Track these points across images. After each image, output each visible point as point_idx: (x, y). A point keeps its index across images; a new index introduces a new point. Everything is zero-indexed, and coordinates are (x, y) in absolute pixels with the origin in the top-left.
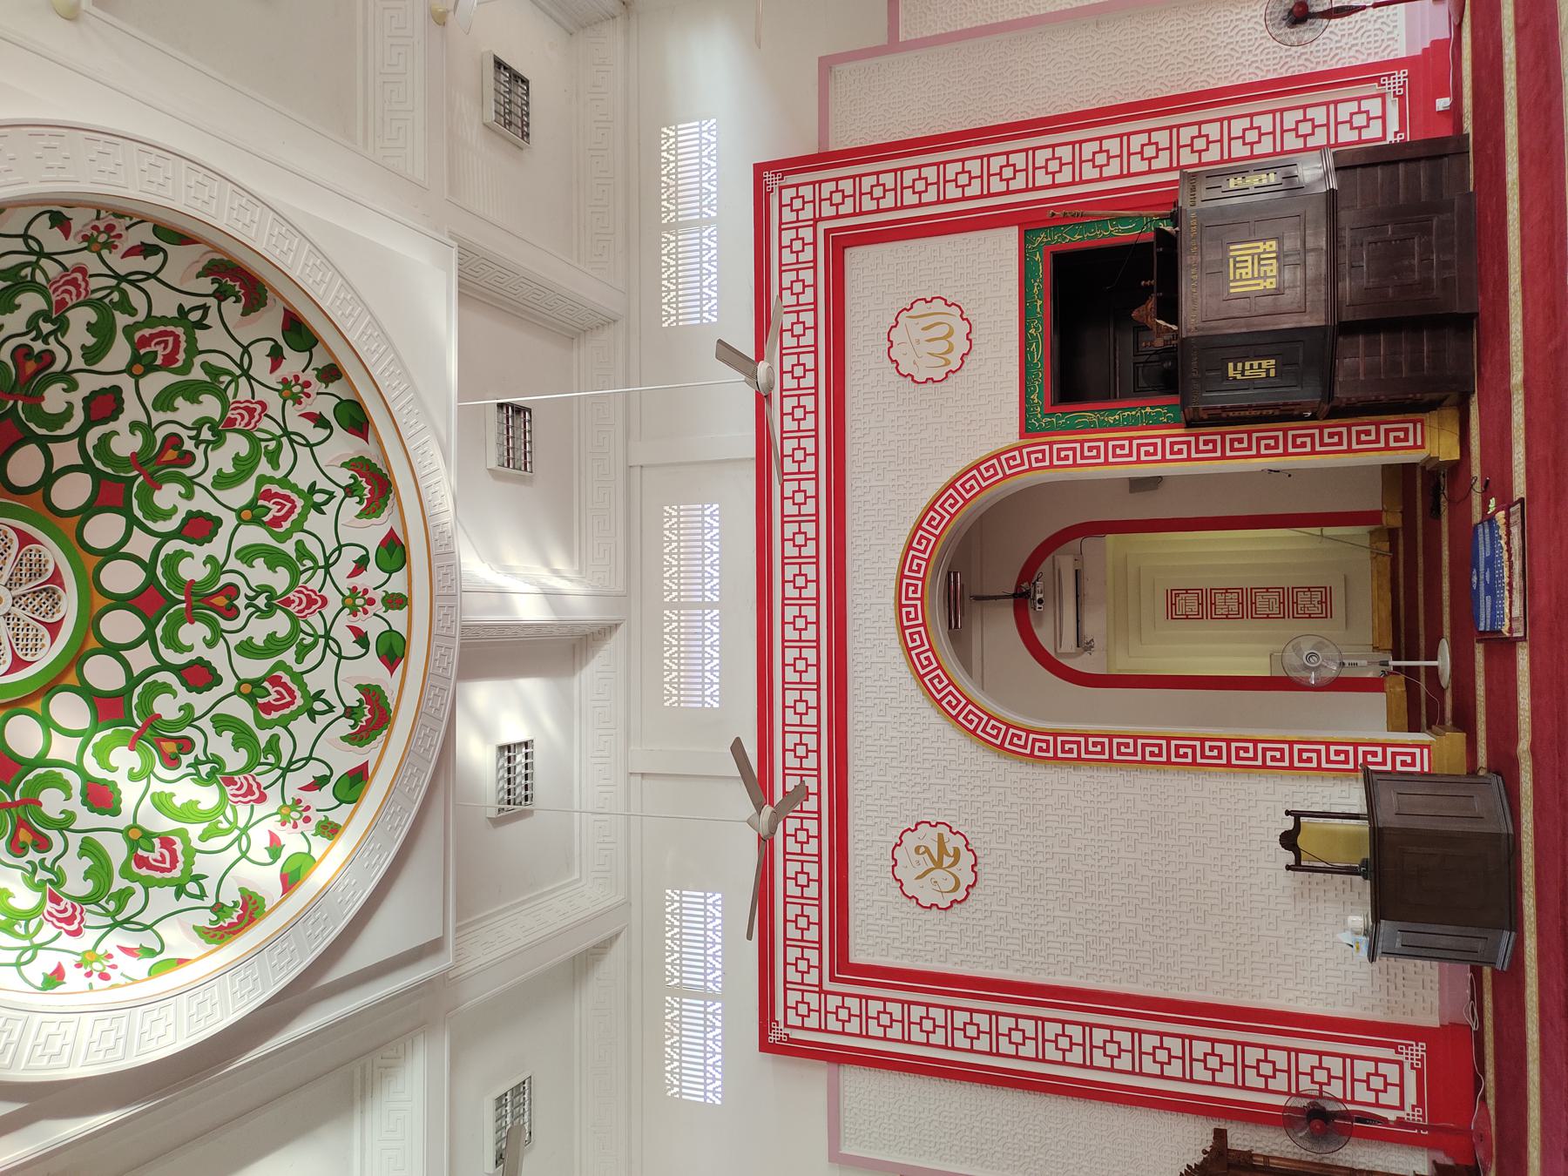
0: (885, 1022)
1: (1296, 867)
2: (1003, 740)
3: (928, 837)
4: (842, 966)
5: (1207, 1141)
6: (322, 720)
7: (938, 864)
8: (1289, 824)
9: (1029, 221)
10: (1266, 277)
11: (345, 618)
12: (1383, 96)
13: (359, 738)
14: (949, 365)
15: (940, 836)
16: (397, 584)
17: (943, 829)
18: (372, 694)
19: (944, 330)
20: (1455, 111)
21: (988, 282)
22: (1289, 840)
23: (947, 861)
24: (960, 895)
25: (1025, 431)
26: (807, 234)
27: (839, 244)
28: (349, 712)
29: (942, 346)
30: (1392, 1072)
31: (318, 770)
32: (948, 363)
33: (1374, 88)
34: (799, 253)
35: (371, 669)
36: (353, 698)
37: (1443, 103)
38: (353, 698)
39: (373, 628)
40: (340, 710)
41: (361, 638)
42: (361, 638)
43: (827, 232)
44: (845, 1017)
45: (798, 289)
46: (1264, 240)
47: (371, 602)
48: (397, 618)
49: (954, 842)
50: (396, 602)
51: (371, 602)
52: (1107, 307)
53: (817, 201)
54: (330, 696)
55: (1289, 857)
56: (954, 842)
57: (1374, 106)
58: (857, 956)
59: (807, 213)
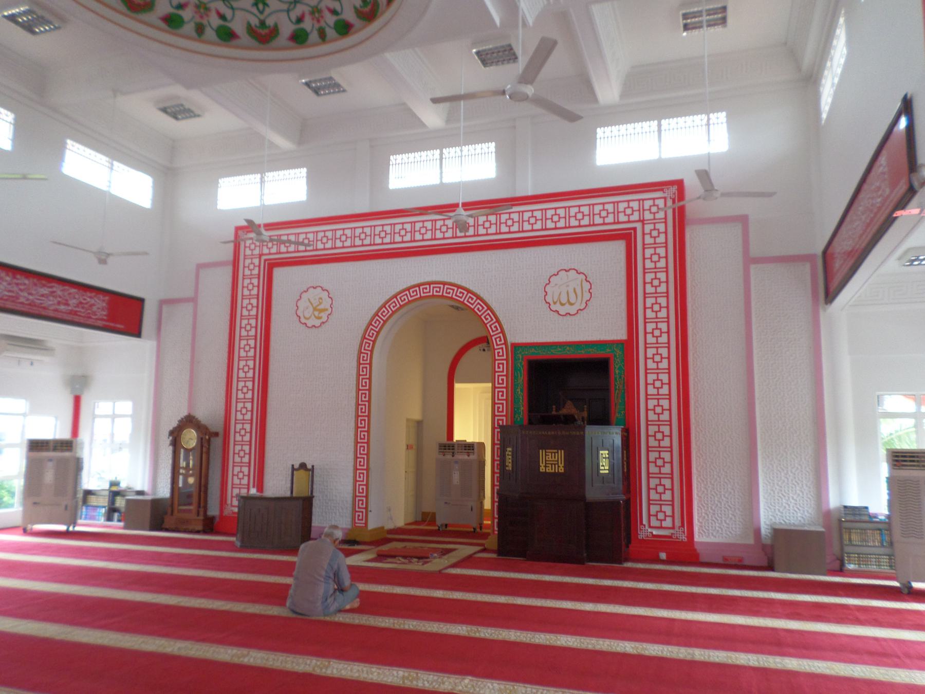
0: (250, 287)
1: (293, 469)
2: (368, 339)
3: (326, 303)
4: (272, 265)
5: (213, 429)
6: (254, 10)
7: (315, 309)
8: (309, 467)
9: (629, 346)
10: (546, 467)
11: (307, 9)
12: (673, 528)
13: (251, 31)
14: (555, 301)
15: (327, 310)
16: (331, 33)
17: (329, 312)
18: (274, 32)
19: (573, 300)
20: (658, 561)
21: (596, 323)
22: (303, 466)
23: (316, 313)
24: (303, 320)
25: (513, 345)
26: (635, 217)
27: (627, 237)
28: (263, 23)
29: (564, 300)
30: (654, 522)
31: (228, 13)
32: (555, 303)
33: (678, 523)
34: (624, 212)
35: (287, 28)
36: (270, 22)
37: (663, 556)
38: (270, 22)
39: (307, 25)
40: (262, 17)
41: (300, 20)
42: (300, 20)
43: (635, 229)
44: (251, 268)
45: (603, 214)
46: (564, 467)
47: (318, 21)
48: (314, 37)
49: (324, 316)
50: (322, 35)
51: (318, 21)
52: (565, 390)
53: (654, 222)
54: (268, 11)
55: (296, 466)
56: (324, 316)
57: (668, 523)
58: (278, 272)
59: (648, 216)
